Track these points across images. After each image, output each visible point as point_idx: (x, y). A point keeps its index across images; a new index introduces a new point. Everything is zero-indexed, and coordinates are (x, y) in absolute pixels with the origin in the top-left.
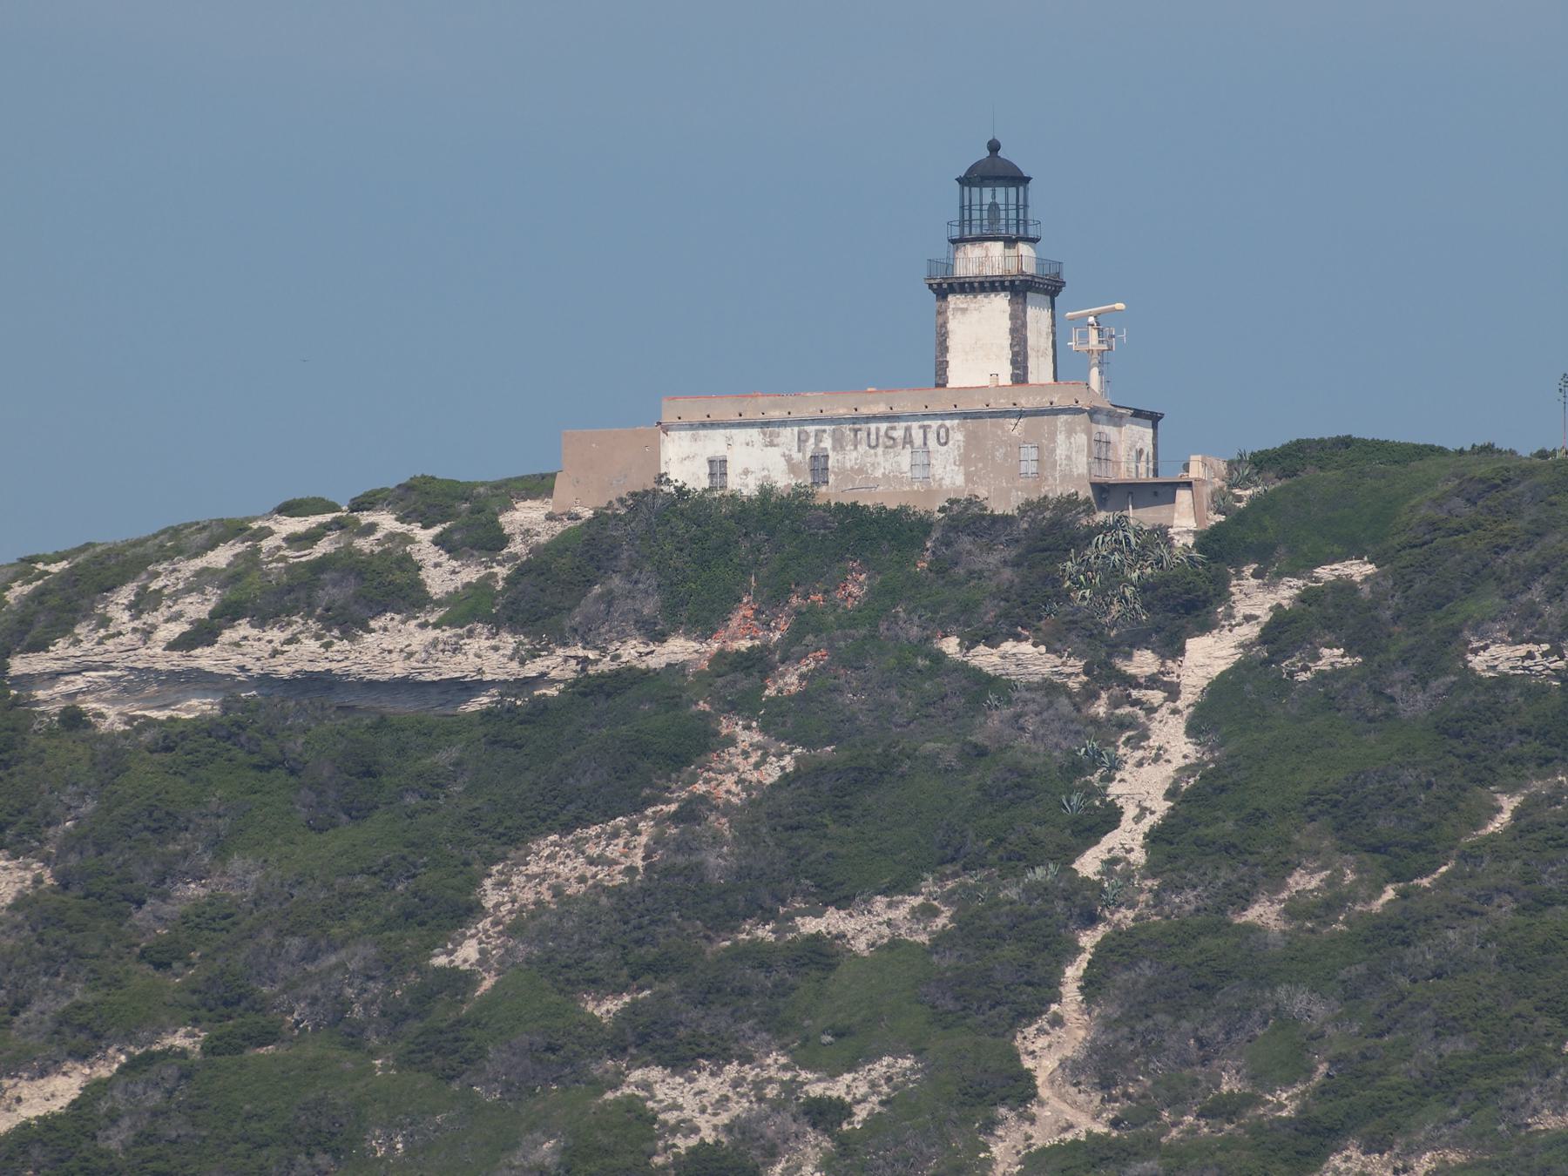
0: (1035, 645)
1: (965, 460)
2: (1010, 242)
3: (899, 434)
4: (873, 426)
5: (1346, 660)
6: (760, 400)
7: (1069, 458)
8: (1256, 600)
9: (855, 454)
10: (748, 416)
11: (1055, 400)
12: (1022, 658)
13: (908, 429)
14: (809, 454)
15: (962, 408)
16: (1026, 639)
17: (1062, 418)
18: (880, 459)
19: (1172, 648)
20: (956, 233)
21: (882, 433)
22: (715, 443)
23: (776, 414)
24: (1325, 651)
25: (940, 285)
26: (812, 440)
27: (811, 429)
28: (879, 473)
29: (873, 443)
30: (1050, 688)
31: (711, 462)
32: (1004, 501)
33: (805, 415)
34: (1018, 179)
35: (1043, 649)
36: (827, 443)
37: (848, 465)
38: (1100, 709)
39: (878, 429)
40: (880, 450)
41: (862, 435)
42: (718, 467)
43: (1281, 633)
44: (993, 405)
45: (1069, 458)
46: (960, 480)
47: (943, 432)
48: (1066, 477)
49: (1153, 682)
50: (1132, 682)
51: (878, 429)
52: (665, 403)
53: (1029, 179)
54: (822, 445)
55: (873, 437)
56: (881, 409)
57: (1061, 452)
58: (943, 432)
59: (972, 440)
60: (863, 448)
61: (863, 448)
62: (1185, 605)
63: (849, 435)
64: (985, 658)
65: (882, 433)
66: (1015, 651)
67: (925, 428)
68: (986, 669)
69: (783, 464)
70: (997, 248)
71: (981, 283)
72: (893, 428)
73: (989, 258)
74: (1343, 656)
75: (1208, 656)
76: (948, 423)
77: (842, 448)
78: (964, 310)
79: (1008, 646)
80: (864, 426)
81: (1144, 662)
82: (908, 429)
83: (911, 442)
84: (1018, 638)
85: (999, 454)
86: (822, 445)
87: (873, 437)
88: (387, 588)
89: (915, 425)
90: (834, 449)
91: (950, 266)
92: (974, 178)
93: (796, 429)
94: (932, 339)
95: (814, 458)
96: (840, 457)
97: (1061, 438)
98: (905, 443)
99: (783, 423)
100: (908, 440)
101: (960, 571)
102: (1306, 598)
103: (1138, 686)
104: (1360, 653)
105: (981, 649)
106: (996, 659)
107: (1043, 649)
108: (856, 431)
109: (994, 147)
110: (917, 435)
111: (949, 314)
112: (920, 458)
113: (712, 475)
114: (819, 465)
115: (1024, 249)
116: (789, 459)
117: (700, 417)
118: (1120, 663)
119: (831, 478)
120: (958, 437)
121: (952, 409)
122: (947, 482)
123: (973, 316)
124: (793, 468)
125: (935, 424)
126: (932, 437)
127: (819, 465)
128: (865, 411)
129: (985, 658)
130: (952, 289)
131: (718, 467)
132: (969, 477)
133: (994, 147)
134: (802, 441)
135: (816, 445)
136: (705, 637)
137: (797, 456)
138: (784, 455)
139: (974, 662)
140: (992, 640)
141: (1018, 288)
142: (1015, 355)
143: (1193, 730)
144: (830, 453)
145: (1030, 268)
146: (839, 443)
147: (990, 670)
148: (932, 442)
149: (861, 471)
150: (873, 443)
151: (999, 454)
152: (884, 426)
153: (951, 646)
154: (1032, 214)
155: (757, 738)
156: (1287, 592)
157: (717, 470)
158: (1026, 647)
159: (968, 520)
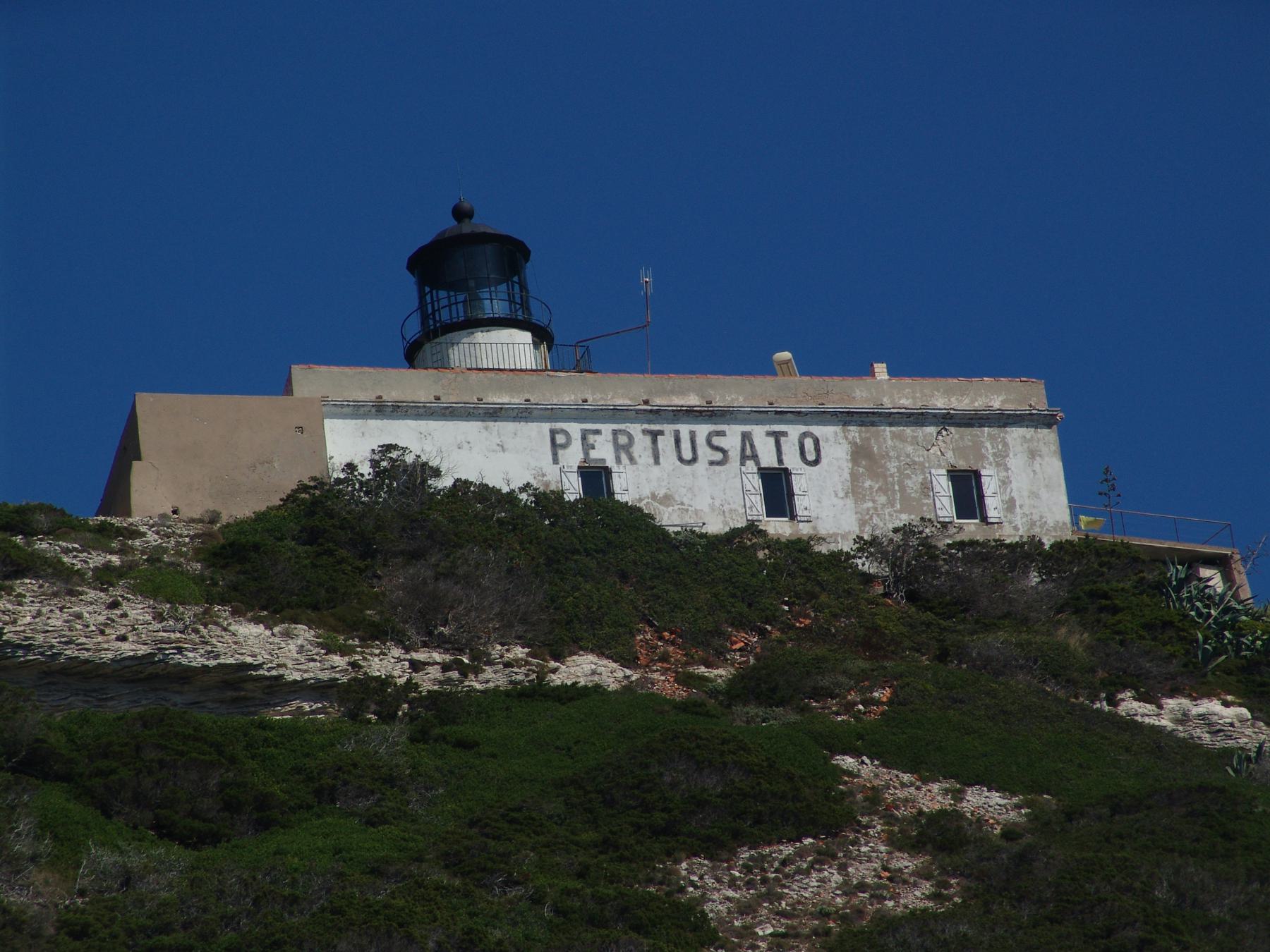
1: (855, 490)
4: (684, 429)
7: (1034, 495)
13: (746, 437)
17: (1015, 434)
21: (701, 440)
27: (575, 429)
29: (687, 455)
41: (666, 443)
47: (809, 443)
54: (594, 454)
58: (809, 443)
59: (859, 453)
63: (642, 445)
67: (777, 436)
72: (721, 434)
76: (817, 430)
80: (668, 428)
86: (594, 454)
88: (166, 929)
93: (546, 427)
98: (743, 458)
99: (524, 414)
108: (655, 435)
117: (367, 396)
125: (794, 431)
142: (952, 416)
146: (624, 449)
150: (687, 455)
152: (703, 430)
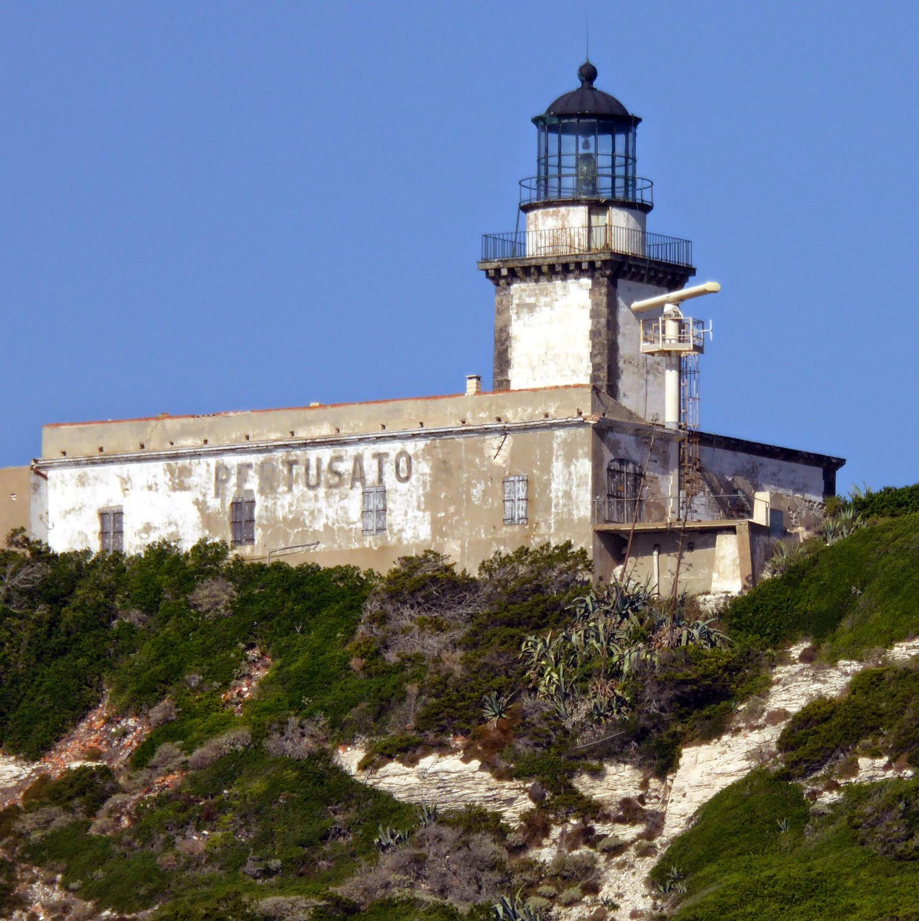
0: (466, 760)
1: (431, 502)
2: (597, 207)
3: (345, 467)
5: (890, 774)
6: (169, 423)
7: (567, 495)
8: (795, 687)
9: (288, 498)
10: (153, 446)
11: (552, 411)
12: (448, 777)
14: (229, 500)
15: (430, 427)
16: (454, 752)
17: (560, 433)
18: (322, 504)
19: (663, 763)
20: (530, 195)
21: (325, 466)
22: (106, 486)
23: (188, 443)
24: (864, 762)
25: (498, 270)
26: (233, 480)
27: (232, 461)
28: (319, 526)
29: (313, 481)
30: (477, 820)
31: (103, 515)
32: (463, 556)
33: (226, 444)
34: (618, 121)
35: (476, 763)
36: (253, 483)
37: (280, 514)
38: (546, 854)
39: (319, 461)
40: (322, 491)
42: (111, 520)
43: (817, 737)
44: (469, 421)
45: (567, 495)
46: (425, 532)
48: (564, 523)
49: (630, 811)
50: (592, 810)
51: (319, 461)
52: (47, 432)
53: (637, 120)
54: (248, 486)
55: (313, 472)
56: (325, 430)
57: (557, 487)
60: (299, 488)
61: (299, 488)
62: (704, 700)
64: (397, 779)
65: (325, 466)
66: (437, 767)
67: (380, 457)
68: (397, 796)
69: (194, 515)
70: (578, 216)
71: (552, 267)
72: (339, 459)
73: (558, 229)
74: (887, 767)
75: (709, 769)
77: (273, 490)
78: (531, 308)
79: (428, 762)
81: (619, 781)
82: (358, 459)
83: (362, 479)
84: (443, 749)
85: (477, 492)
86: (248, 486)
87: (313, 472)
89: (367, 450)
90: (262, 491)
91: (518, 243)
92: (556, 120)
94: (490, 351)
95: (236, 505)
96: (270, 503)
97: (558, 466)
98: (354, 479)
100: (358, 475)
101: (392, 657)
102: (863, 685)
103: (606, 818)
104: (912, 762)
105: (394, 766)
106: (413, 780)
107: (476, 763)
108: (290, 464)
109: (589, 74)
110: (370, 468)
111: (513, 313)
112: (374, 503)
113: (103, 534)
114: (242, 516)
115: (619, 218)
116: (201, 505)
117: (89, 449)
118: (583, 783)
119: (258, 534)
120: (423, 468)
121: (416, 429)
122: (407, 536)
123: (543, 314)
124: (208, 519)
125: (392, 448)
126: (389, 469)
127: (242, 516)
128: (303, 434)
129: (397, 779)
130: (513, 275)
131: (111, 520)
132: (437, 527)
133: (589, 74)
134: (220, 484)
135: (239, 486)
136: (33, 756)
137: (214, 503)
138: (197, 502)
139: (383, 785)
140: (408, 752)
141: (618, 273)
143: (658, 879)
144: (258, 498)
145: (621, 245)
146: (268, 485)
147: (401, 796)
148: (390, 479)
149: (296, 522)
150: (313, 481)
151: (477, 492)
152: (326, 454)
153: (350, 758)
154: (642, 169)
155: (57, 895)
156: (835, 682)
157: (110, 526)
158: (452, 763)
159: (425, 583)
